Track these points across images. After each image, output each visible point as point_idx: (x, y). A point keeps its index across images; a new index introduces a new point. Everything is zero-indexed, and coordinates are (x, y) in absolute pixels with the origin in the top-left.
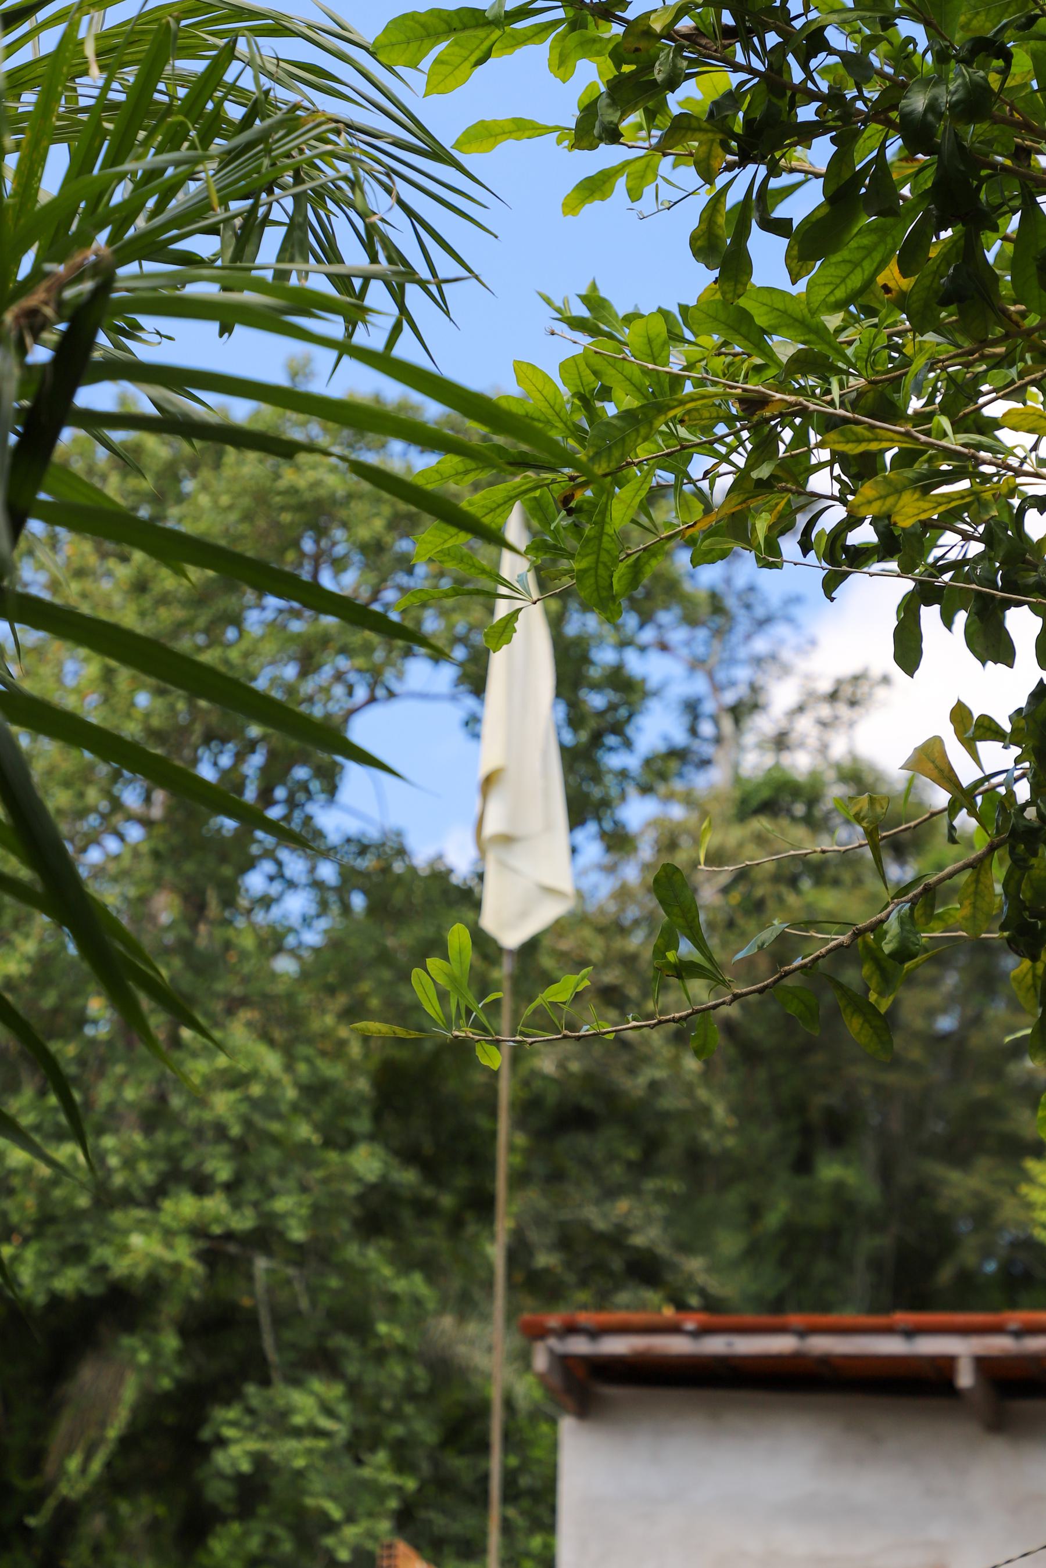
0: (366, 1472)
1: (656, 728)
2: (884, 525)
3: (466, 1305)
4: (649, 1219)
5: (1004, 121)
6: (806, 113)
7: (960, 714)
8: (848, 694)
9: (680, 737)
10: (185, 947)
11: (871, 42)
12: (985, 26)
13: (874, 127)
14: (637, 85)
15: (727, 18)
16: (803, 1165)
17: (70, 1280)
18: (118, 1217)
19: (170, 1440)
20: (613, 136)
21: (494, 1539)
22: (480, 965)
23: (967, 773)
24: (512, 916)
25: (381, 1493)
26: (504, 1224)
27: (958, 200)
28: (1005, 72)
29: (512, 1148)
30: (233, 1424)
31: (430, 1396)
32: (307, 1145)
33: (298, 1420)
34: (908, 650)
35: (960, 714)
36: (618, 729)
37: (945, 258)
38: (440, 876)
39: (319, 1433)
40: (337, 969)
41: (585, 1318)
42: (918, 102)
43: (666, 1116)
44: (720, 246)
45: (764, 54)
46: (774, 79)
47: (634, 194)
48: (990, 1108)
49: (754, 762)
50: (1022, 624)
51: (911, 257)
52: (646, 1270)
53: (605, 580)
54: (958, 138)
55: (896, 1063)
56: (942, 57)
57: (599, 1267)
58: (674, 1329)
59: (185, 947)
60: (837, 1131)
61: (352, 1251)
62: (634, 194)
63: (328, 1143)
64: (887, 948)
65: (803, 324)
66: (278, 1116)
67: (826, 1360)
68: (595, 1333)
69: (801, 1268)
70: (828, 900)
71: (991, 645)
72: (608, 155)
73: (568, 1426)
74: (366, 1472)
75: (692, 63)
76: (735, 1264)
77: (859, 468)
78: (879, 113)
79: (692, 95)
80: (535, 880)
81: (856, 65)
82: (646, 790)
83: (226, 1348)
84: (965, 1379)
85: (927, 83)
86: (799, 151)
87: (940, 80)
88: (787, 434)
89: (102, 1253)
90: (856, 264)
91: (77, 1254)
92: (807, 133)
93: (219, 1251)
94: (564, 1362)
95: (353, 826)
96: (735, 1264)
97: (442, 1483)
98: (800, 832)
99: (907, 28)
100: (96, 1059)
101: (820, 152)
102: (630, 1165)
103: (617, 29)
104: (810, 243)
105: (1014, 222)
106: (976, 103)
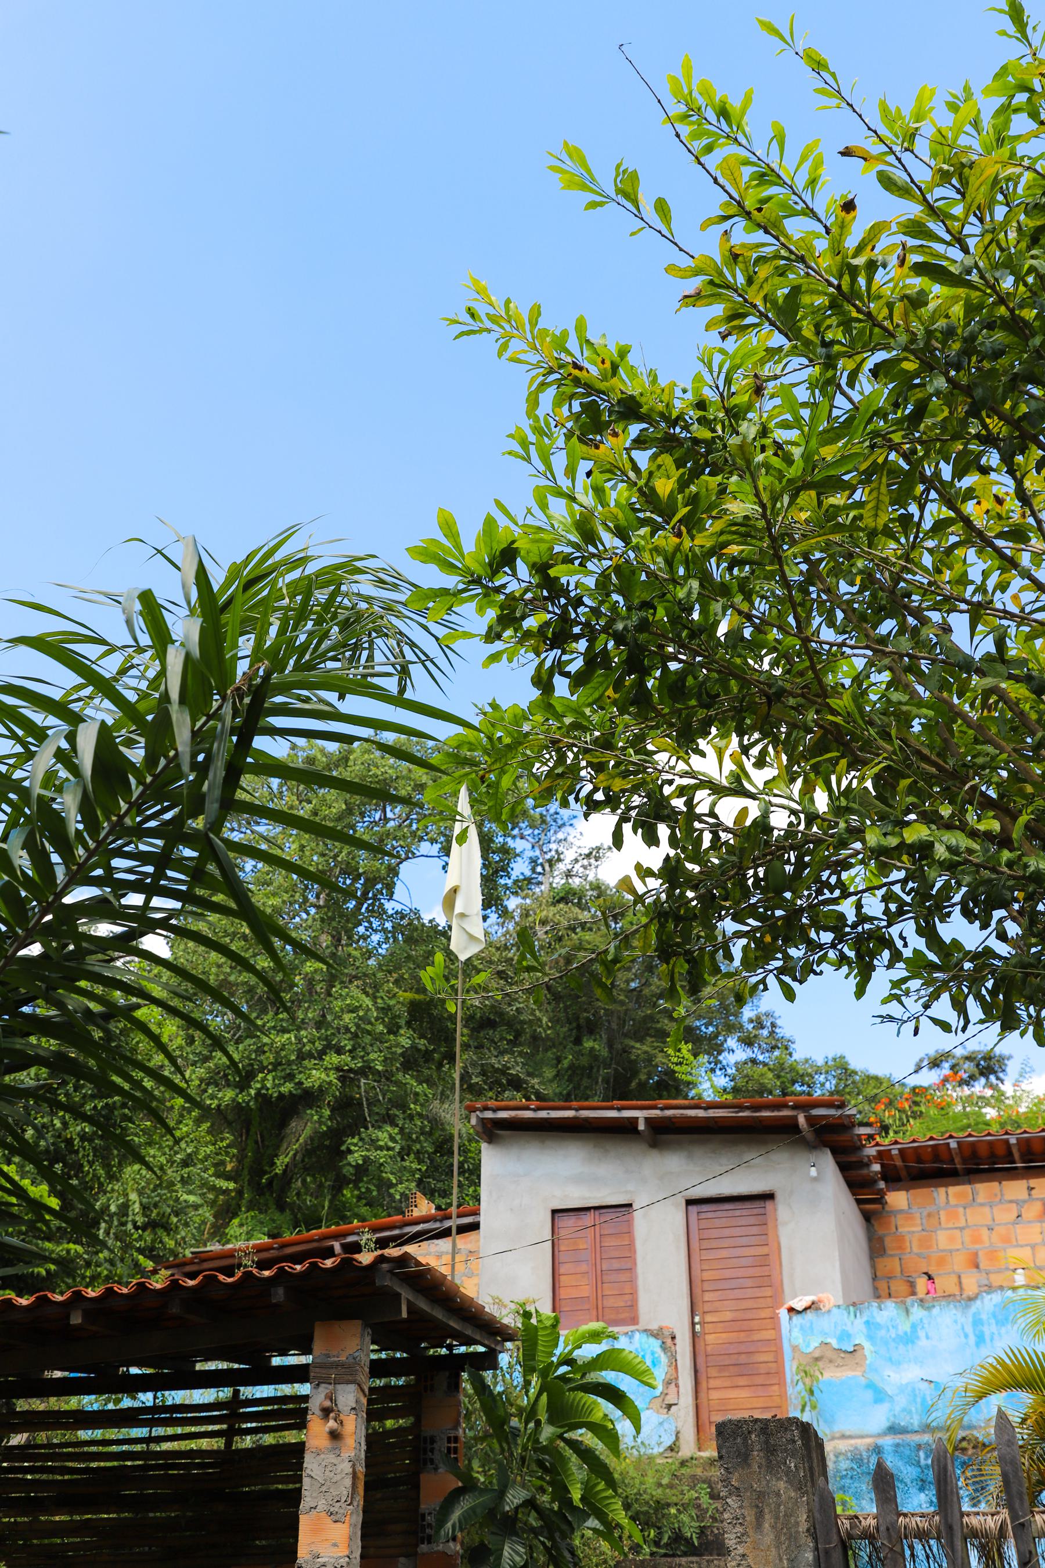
0: (407, 1164)
1: (520, 868)
2: (607, 791)
3: (444, 1097)
4: (517, 1063)
5: (656, 634)
6: (577, 630)
7: (638, 867)
8: (594, 855)
9: (528, 873)
10: (333, 955)
11: (602, 602)
12: (646, 596)
13: (603, 636)
14: (509, 618)
15: (545, 593)
16: (578, 1041)
17: (287, 1088)
18: (306, 1062)
19: (327, 1152)
20: (499, 637)
21: (455, 1190)
22: (448, 963)
23: (641, 889)
24: (463, 949)
25: (413, 1173)
26: (459, 1064)
27: (636, 664)
28: (654, 614)
29: (462, 1035)
30: (355, 1145)
31: (430, 1134)
32: (381, 1033)
33: (381, 1143)
34: (618, 840)
35: (638, 867)
36: (504, 869)
37: (632, 686)
38: (434, 927)
39: (389, 1149)
40: (391, 964)
41: (492, 1103)
42: (620, 626)
43: (523, 1022)
44: (543, 682)
45: (560, 607)
46: (564, 617)
47: (510, 661)
48: (651, 1018)
49: (558, 881)
50: (663, 831)
51: (618, 686)
52: (516, 1084)
53: (498, 812)
54: (636, 640)
55: (614, 1001)
56: (629, 609)
57: (498, 1082)
58: (527, 1108)
59: (333, 955)
60: (592, 1028)
61: (400, 1076)
62: (510, 661)
63: (389, 1032)
64: (609, 958)
65: (578, 712)
66: (370, 1023)
67: (587, 1120)
68: (495, 1110)
69: (577, 1083)
70: (587, 936)
71: (652, 840)
72: (498, 646)
73: (484, 1146)
74: (407, 1164)
75: (531, 610)
76: (551, 1081)
77: (599, 768)
78: (605, 630)
79: (531, 623)
80: (471, 933)
81: (595, 611)
82: (516, 894)
83: (350, 1115)
84: (641, 1127)
85: (623, 619)
86: (574, 645)
87: (628, 618)
88: (570, 755)
89: (300, 1077)
90: (596, 689)
91: (290, 1077)
92: (577, 638)
93: (346, 1076)
94: (483, 1121)
95: (399, 907)
96: (551, 1081)
97: (434, 1169)
98: (576, 910)
99: (615, 597)
100: (297, 1001)
101: (582, 645)
102: (509, 1042)
103: (502, 597)
104: (578, 681)
105: (658, 673)
106: (644, 626)
